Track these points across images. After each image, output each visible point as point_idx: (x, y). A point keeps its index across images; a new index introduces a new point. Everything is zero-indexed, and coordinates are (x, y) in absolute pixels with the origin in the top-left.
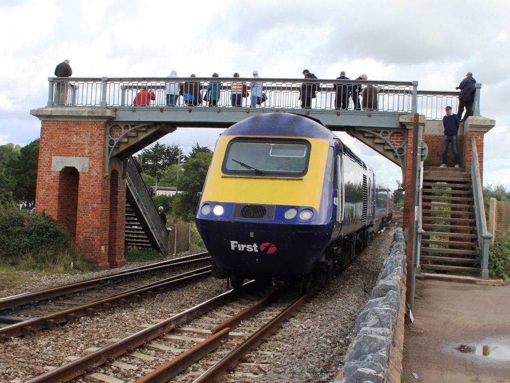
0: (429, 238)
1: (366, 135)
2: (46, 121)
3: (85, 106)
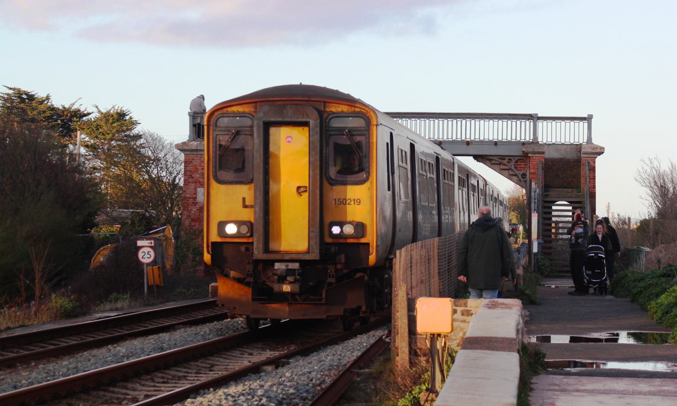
1: (493, 162)
2: (190, 154)
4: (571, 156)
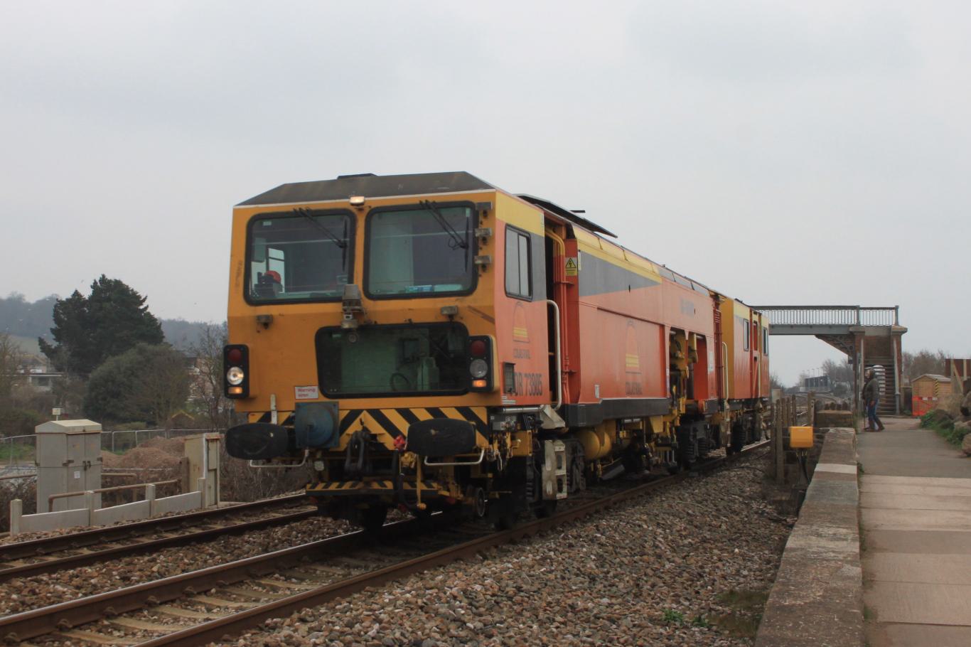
4: (883, 333)
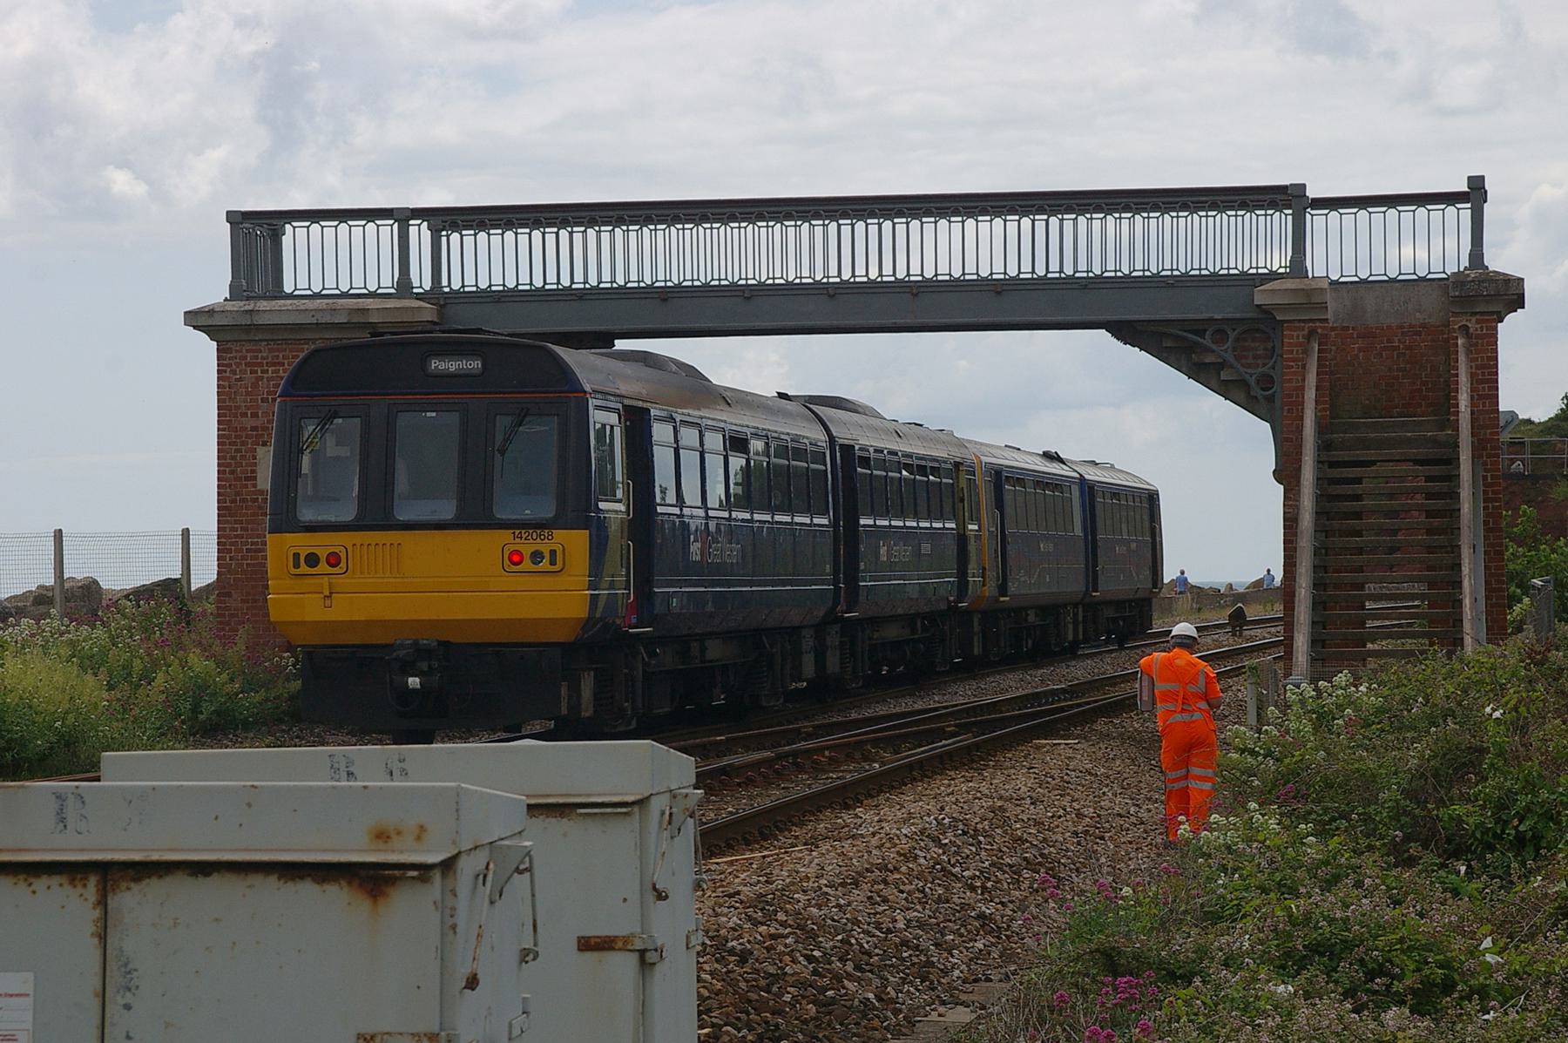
0: (1363, 588)
3: (345, 295)
